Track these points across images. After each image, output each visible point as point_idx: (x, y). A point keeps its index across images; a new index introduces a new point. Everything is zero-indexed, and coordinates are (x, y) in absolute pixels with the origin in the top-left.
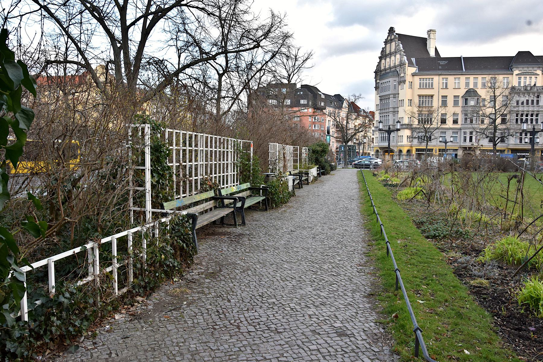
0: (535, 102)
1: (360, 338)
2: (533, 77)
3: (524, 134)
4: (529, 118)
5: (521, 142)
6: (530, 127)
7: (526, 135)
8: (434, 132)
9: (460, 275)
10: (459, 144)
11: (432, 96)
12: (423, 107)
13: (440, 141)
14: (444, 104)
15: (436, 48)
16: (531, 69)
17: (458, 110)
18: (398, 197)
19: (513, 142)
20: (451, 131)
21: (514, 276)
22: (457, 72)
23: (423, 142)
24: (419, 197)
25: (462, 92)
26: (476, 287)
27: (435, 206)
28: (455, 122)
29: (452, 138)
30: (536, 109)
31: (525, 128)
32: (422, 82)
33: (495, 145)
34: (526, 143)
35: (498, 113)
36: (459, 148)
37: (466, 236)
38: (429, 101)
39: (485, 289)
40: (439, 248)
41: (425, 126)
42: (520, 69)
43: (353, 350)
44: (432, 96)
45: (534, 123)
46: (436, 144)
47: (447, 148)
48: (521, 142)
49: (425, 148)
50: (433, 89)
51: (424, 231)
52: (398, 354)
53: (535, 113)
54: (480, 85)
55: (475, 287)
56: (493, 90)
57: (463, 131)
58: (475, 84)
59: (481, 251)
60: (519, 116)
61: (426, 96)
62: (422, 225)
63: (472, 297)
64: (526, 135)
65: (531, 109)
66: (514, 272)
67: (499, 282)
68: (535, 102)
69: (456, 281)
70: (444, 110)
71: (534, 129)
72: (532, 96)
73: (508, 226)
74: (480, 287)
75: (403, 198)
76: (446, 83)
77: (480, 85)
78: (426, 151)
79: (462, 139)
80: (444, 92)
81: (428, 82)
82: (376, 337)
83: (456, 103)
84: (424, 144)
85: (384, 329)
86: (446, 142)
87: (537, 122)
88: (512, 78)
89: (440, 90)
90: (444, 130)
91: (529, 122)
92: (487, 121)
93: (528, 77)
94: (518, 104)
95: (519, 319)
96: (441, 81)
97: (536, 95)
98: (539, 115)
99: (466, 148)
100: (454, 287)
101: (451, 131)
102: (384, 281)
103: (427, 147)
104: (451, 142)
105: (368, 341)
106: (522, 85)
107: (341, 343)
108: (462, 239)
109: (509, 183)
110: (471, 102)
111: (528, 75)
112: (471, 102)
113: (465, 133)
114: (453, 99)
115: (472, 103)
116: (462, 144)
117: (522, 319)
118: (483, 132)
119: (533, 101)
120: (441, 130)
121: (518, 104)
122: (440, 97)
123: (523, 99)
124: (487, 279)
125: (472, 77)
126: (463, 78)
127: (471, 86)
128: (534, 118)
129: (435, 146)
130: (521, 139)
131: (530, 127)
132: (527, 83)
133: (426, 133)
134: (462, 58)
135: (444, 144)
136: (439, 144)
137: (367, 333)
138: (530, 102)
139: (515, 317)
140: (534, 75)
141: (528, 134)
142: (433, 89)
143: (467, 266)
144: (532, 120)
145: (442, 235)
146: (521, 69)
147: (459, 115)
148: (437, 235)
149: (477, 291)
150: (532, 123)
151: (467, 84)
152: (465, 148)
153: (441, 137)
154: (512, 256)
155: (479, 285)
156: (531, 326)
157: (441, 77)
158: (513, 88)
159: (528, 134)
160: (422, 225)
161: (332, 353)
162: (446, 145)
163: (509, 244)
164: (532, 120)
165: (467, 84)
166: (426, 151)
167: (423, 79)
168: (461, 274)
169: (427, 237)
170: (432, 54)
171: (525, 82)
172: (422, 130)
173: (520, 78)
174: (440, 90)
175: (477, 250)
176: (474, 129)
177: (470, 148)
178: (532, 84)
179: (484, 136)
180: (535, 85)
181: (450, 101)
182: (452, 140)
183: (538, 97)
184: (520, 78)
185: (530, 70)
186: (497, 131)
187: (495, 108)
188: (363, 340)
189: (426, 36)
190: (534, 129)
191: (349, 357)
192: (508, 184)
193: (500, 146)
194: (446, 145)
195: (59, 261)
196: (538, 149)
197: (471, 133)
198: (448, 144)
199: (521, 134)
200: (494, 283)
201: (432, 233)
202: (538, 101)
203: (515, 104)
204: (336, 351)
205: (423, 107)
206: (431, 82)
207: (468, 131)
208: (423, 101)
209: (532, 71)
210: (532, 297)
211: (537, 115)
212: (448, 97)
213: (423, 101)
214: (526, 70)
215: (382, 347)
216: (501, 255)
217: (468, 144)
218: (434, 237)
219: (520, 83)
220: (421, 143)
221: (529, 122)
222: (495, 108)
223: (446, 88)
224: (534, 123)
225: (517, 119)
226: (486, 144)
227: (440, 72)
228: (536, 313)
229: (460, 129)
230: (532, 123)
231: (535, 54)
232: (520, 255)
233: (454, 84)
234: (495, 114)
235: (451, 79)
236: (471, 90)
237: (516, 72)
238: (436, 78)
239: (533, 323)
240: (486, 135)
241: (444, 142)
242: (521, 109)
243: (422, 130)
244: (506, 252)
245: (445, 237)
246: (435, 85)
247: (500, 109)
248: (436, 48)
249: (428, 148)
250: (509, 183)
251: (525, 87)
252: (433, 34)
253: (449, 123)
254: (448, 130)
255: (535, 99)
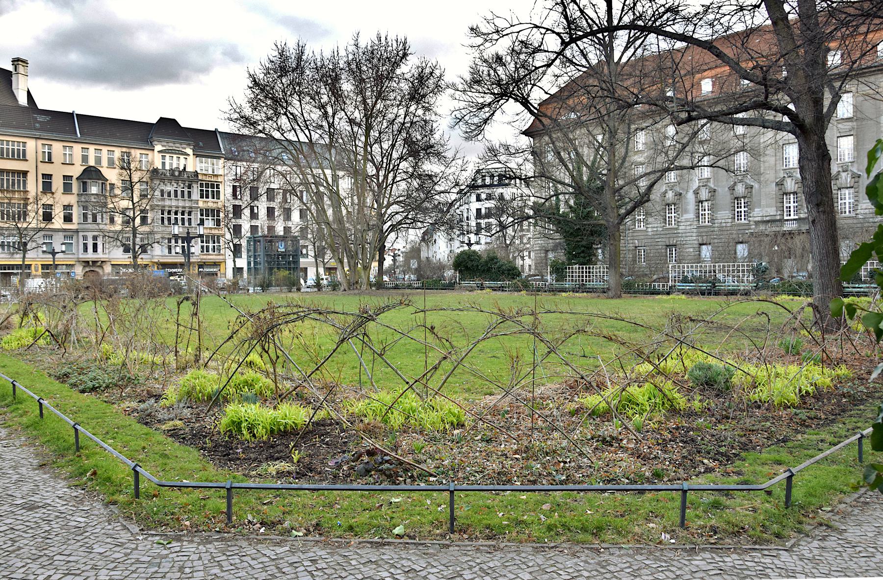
0: (186, 193)
1: (58, 505)
2: (182, 157)
3: (173, 241)
4: (179, 216)
5: (170, 252)
6: (181, 230)
7: (176, 242)
8: (35, 237)
9: (146, 424)
10: (76, 256)
11: (25, 173)
12: (14, 192)
13: (44, 252)
14: (47, 187)
15: (29, 92)
16: (178, 145)
17: (71, 199)
18: (6, 346)
19: (158, 252)
20: (61, 233)
21: (208, 411)
22: (68, 137)
23: (17, 253)
24: (41, 342)
25: (76, 171)
26: (170, 430)
27: (74, 353)
28: (68, 219)
29: (64, 246)
30: (188, 204)
31: (176, 233)
32: (5, 147)
33: (135, 257)
34: (176, 253)
35: (138, 208)
36: (77, 263)
37: (136, 382)
38: (19, 181)
39: (180, 430)
40: (105, 402)
41: (19, 226)
42: (163, 143)
43: (58, 517)
44: (25, 173)
45: (187, 224)
46: (36, 256)
47: (56, 263)
48: (170, 252)
49: (21, 263)
50: (27, 160)
51: (74, 385)
52: (115, 503)
53: (187, 210)
54: (105, 162)
55: (169, 431)
56: (128, 171)
57: (81, 234)
58: (98, 160)
59: (160, 396)
60: (166, 214)
61: (14, 172)
62: (68, 377)
63: (170, 439)
64: (176, 242)
65: (181, 204)
66: (206, 409)
67: (194, 421)
68: (186, 193)
69: (145, 429)
70: (52, 199)
71: (188, 233)
72: (182, 186)
73: (185, 362)
74: (174, 430)
75: (14, 345)
76: (50, 154)
77: (105, 162)
78: (24, 268)
79: (81, 247)
80: (46, 169)
81: (16, 148)
82: (78, 499)
83: (67, 188)
84: (18, 256)
85: (83, 489)
86: (54, 253)
87: (190, 224)
88: (154, 156)
89: (40, 164)
90: (50, 233)
91: (180, 223)
92: (119, 219)
93: (175, 156)
94: (162, 195)
95: (225, 446)
96: (40, 150)
97: (187, 185)
98: (193, 214)
99: (88, 262)
100: (146, 434)
101: (61, 234)
102: (53, 448)
103: (24, 261)
104: (63, 252)
105: (70, 504)
106: (167, 167)
107: (37, 515)
108: (132, 385)
109: (179, 308)
110: (93, 188)
111: (176, 154)
112: (93, 188)
113: (85, 238)
114: (61, 181)
115: (94, 190)
116: (81, 256)
117: (228, 446)
118: (115, 237)
119: (176, 191)
120: (43, 233)
121: (162, 195)
122: (40, 177)
123: (169, 188)
124: (181, 420)
125: (92, 148)
126: (77, 148)
127: (92, 163)
128: (186, 217)
129: (34, 259)
130: (170, 248)
131: (181, 230)
132: (174, 166)
133: (21, 238)
134: (75, 116)
135: (51, 256)
136: (41, 255)
137: (65, 498)
138: (179, 193)
139: (220, 445)
140: (182, 154)
141: (180, 241)
142: (27, 160)
143: (151, 413)
144: (183, 219)
145: (104, 385)
146: (165, 144)
147: (74, 208)
148: (97, 385)
149: (174, 434)
150: (183, 224)
151: (85, 158)
152: (86, 263)
153: (44, 243)
154: (200, 392)
155: (173, 428)
156: (238, 449)
157: (40, 142)
158: (155, 171)
159: (180, 241)
160: (68, 377)
161: (33, 526)
162: (54, 258)
163: (195, 379)
164: (183, 219)
165: (85, 158)
166: (24, 268)
167: (8, 141)
168: (147, 423)
169: (83, 391)
170: (23, 100)
171: (171, 164)
172: (15, 232)
173: (163, 157)
174: (40, 164)
175: (156, 396)
176: (100, 230)
177: (94, 262)
178: (181, 168)
179: (119, 243)
180: (185, 168)
181: (57, 184)
182: (64, 249)
183: (189, 187)
184: (163, 157)
185: (177, 146)
186: (137, 235)
187: (132, 201)
188: (63, 505)
189: (10, 68)
190: (188, 233)
191: (57, 523)
192: (177, 310)
193: (143, 259)
194: (54, 258)
195: (822, 126)
196: (194, 263)
197: (95, 238)
198: (57, 256)
199: (170, 240)
200: (189, 422)
201: (90, 384)
202: (189, 193)
203: (160, 197)
204: (36, 522)
205: (21, 191)
206: (21, 148)
207: (90, 235)
208: (13, 181)
209: (180, 149)
210: (233, 422)
211: (190, 214)
212: (53, 177)
213: (13, 181)
214: (171, 146)
215: (92, 504)
216: (188, 393)
217: (90, 255)
218: (93, 389)
219: (164, 164)
220: (13, 254)
221: (180, 223)
222: (132, 201)
223: (50, 161)
224: (187, 224)
225: (163, 218)
226: (118, 255)
227: (38, 133)
228: (239, 437)
229: (77, 231)
230: (183, 224)
231: (184, 124)
232: (209, 389)
233: (63, 157)
234: (134, 209)
235: (57, 148)
236: (92, 169)
237: (158, 147)
238: (31, 144)
239: (239, 446)
240: (121, 241)
241: (49, 253)
242: (167, 203)
243: (15, 232)
244: (194, 388)
245: (107, 387)
246: (30, 155)
247: (140, 202)
248: (29, 92)
249: (26, 263)
250: (179, 308)
251: (172, 171)
252: (23, 66)
253: (58, 222)
254: (57, 233)
255: (186, 190)
